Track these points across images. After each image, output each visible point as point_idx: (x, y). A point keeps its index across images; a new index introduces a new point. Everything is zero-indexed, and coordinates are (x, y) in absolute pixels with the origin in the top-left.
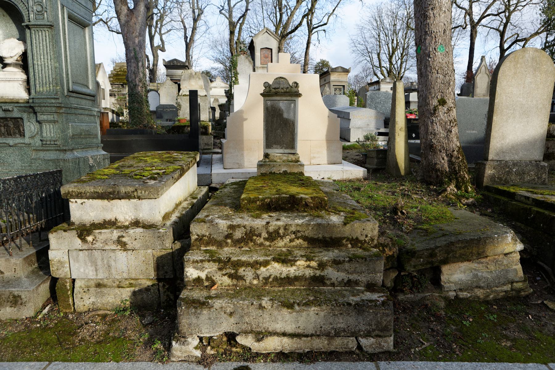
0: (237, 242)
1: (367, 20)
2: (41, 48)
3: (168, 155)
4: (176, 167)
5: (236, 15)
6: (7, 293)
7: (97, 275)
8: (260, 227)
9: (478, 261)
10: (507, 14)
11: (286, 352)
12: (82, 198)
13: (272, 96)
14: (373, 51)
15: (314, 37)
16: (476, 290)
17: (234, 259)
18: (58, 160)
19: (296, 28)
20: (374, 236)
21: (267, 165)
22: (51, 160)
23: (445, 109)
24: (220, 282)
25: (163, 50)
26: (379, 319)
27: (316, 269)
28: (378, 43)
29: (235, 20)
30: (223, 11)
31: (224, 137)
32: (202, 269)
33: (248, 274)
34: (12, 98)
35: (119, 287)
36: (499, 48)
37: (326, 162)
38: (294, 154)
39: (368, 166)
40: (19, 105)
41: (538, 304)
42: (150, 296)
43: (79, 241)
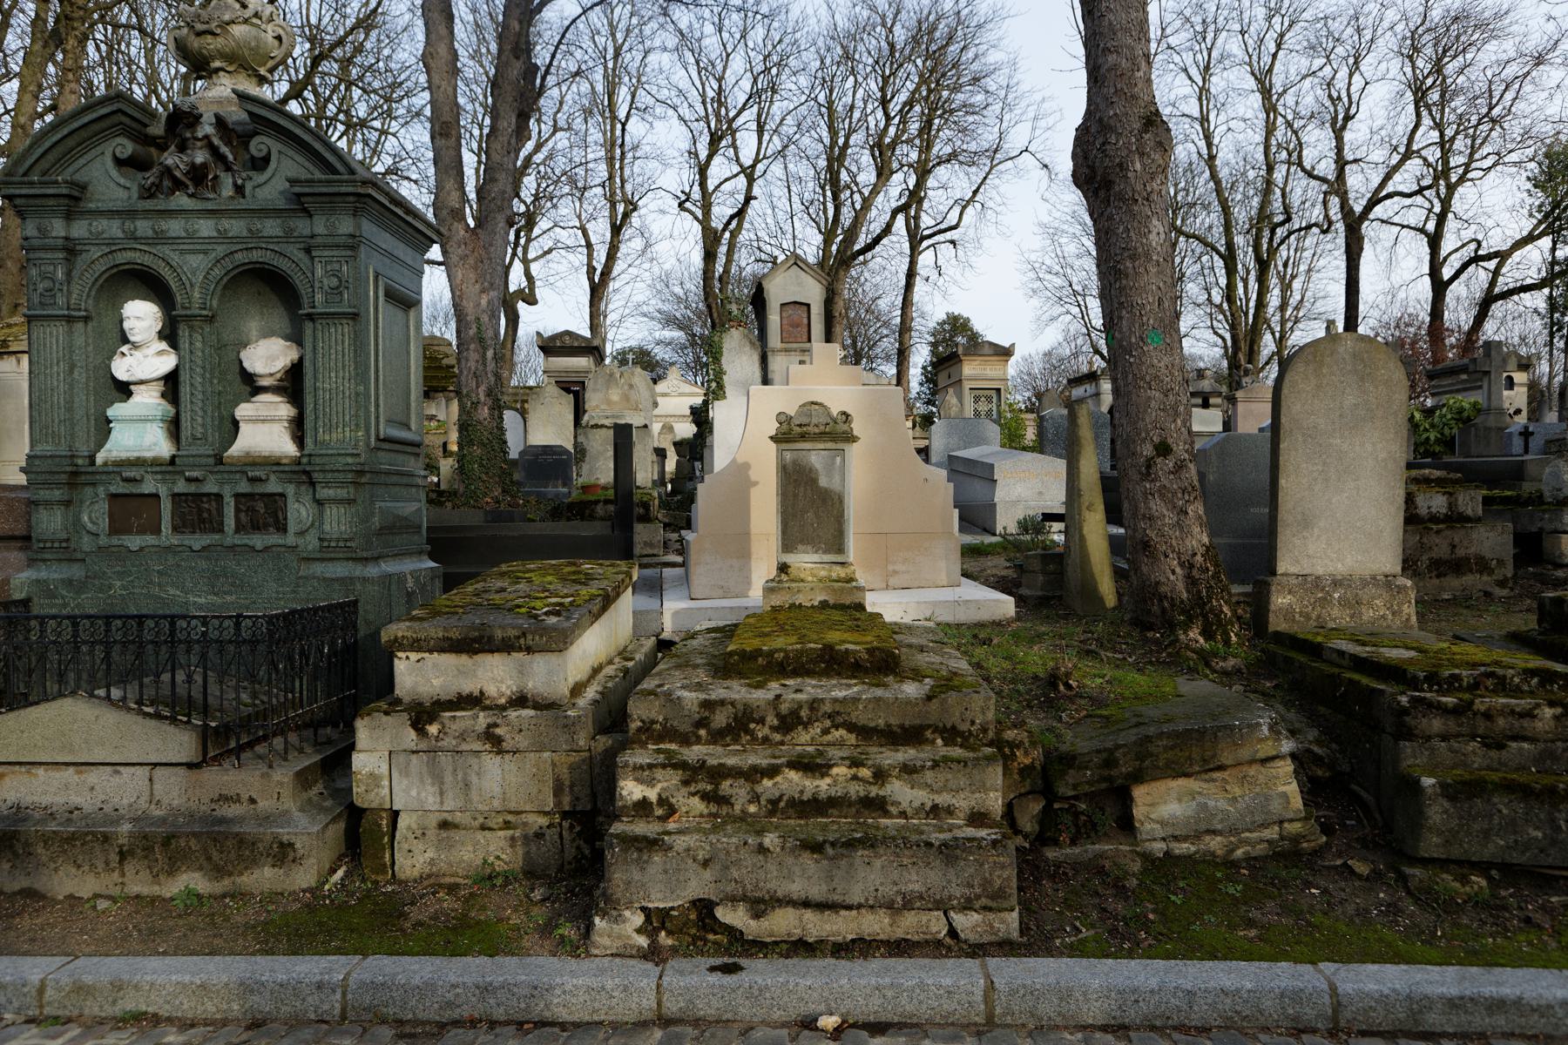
0: (717, 737)
2: (333, 357)
3: (573, 569)
4: (594, 591)
5: (722, 211)
6: (269, 838)
7: (442, 803)
8: (762, 703)
9: (1207, 777)
10: (1443, 190)
11: (811, 940)
12: (419, 650)
15: (925, 259)
16: (1207, 838)
17: (712, 762)
18: (351, 578)
19: (877, 241)
20: (987, 723)
21: (783, 588)
22: (337, 579)
23: (1171, 465)
24: (684, 809)
25: (531, 300)
26: (987, 875)
27: (871, 783)
29: (717, 224)
30: (688, 205)
31: (689, 526)
32: (650, 783)
33: (737, 791)
34: (278, 454)
35: (483, 828)
36: (1427, 280)
38: (842, 563)
39: (1024, 591)
40: (281, 468)
41: (1336, 867)
42: (544, 849)
43: (413, 734)
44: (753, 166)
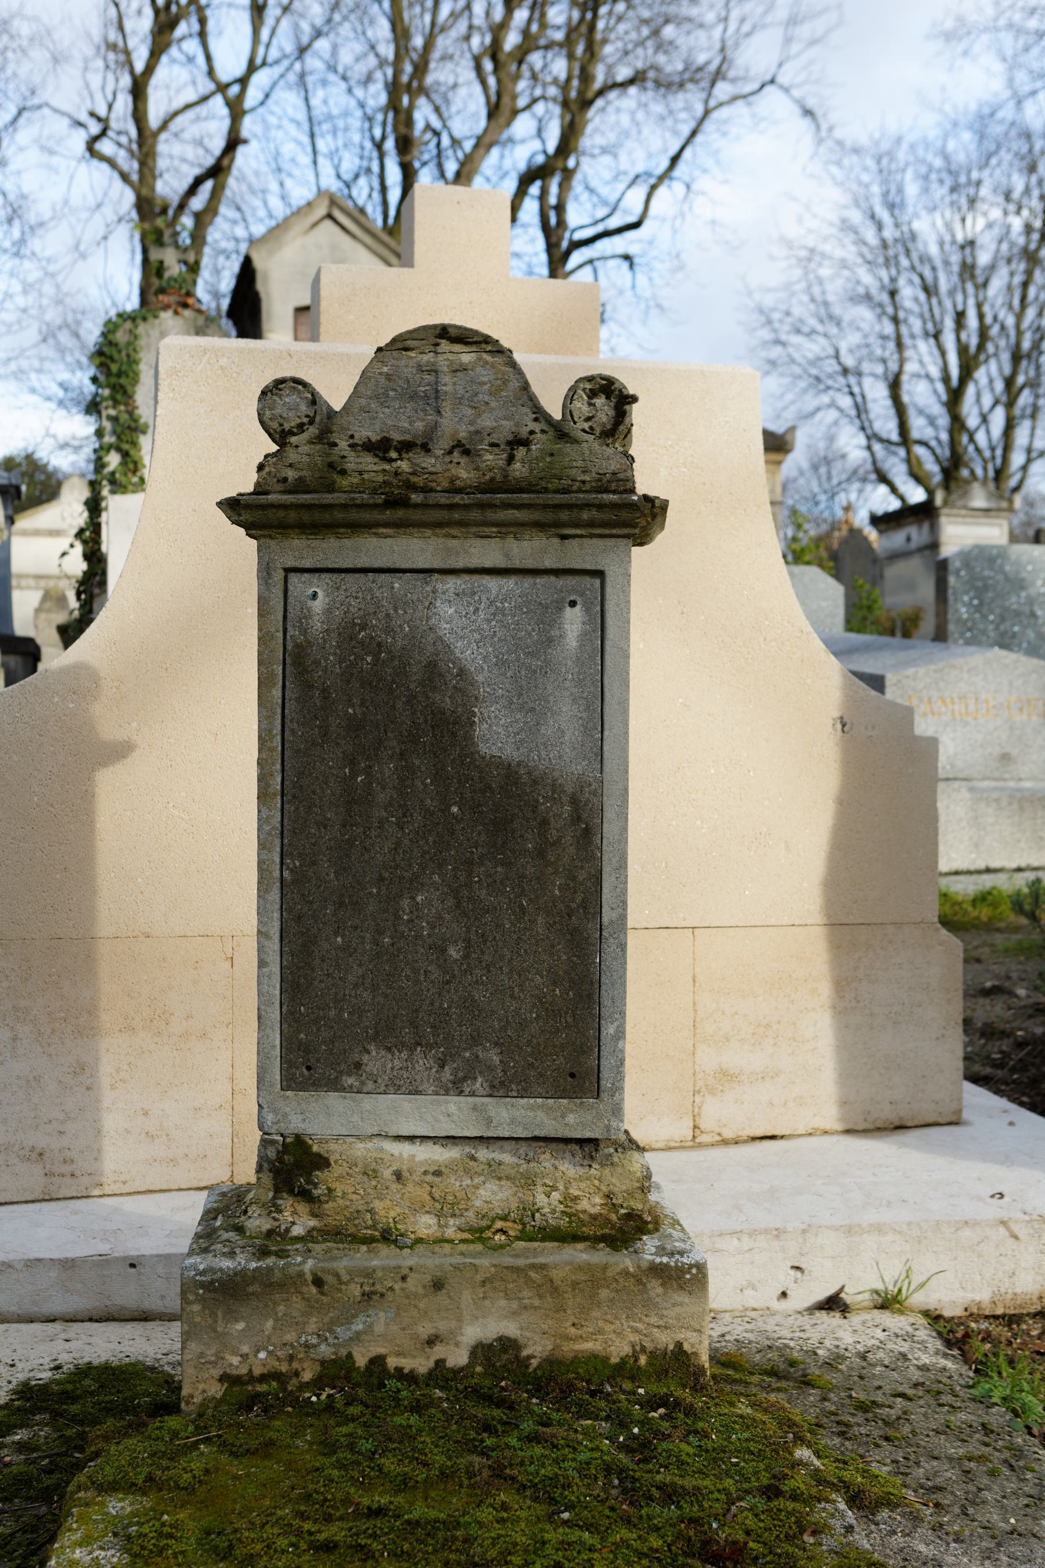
1: (834, 218)
13: (356, 527)
14: (866, 367)
21: (290, 1283)
28: (889, 329)
37: (829, 1116)
44: (243, 81)
